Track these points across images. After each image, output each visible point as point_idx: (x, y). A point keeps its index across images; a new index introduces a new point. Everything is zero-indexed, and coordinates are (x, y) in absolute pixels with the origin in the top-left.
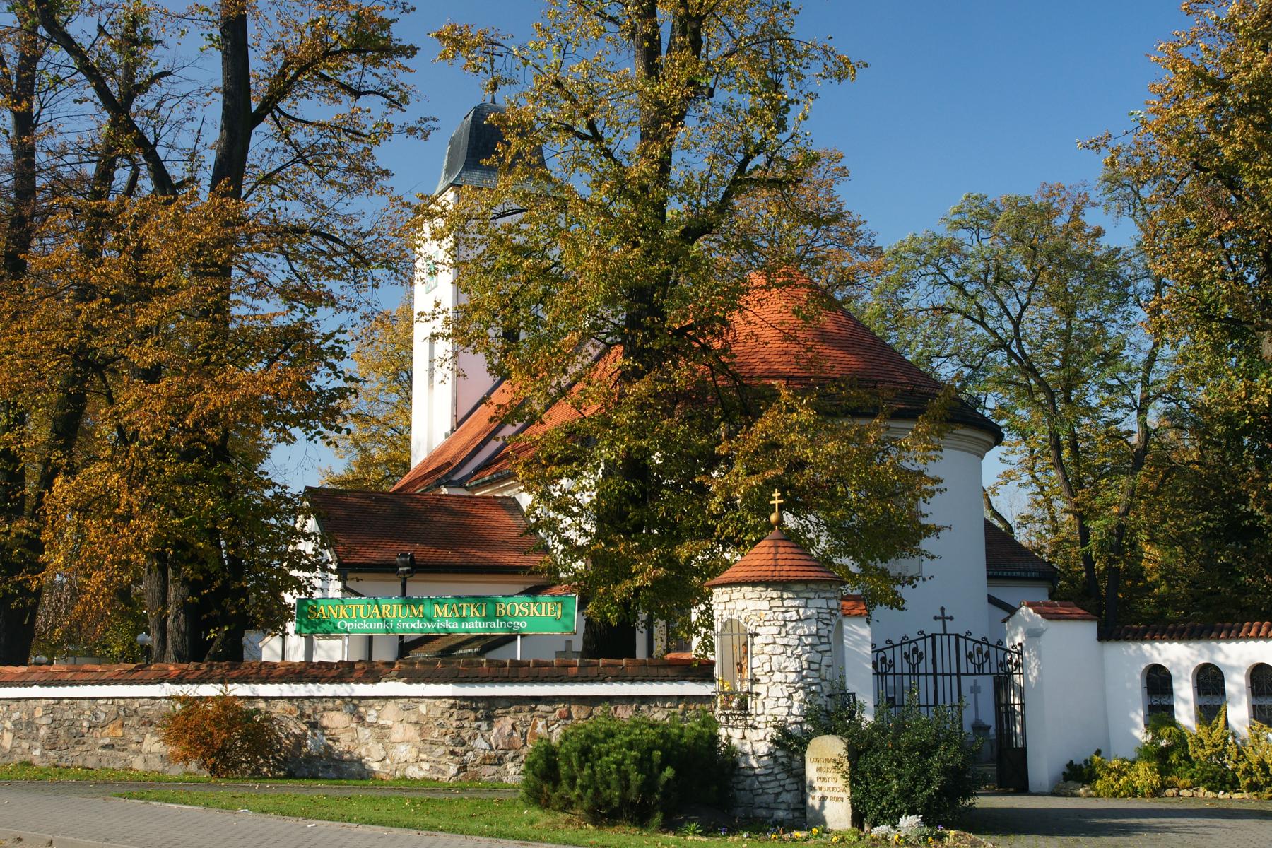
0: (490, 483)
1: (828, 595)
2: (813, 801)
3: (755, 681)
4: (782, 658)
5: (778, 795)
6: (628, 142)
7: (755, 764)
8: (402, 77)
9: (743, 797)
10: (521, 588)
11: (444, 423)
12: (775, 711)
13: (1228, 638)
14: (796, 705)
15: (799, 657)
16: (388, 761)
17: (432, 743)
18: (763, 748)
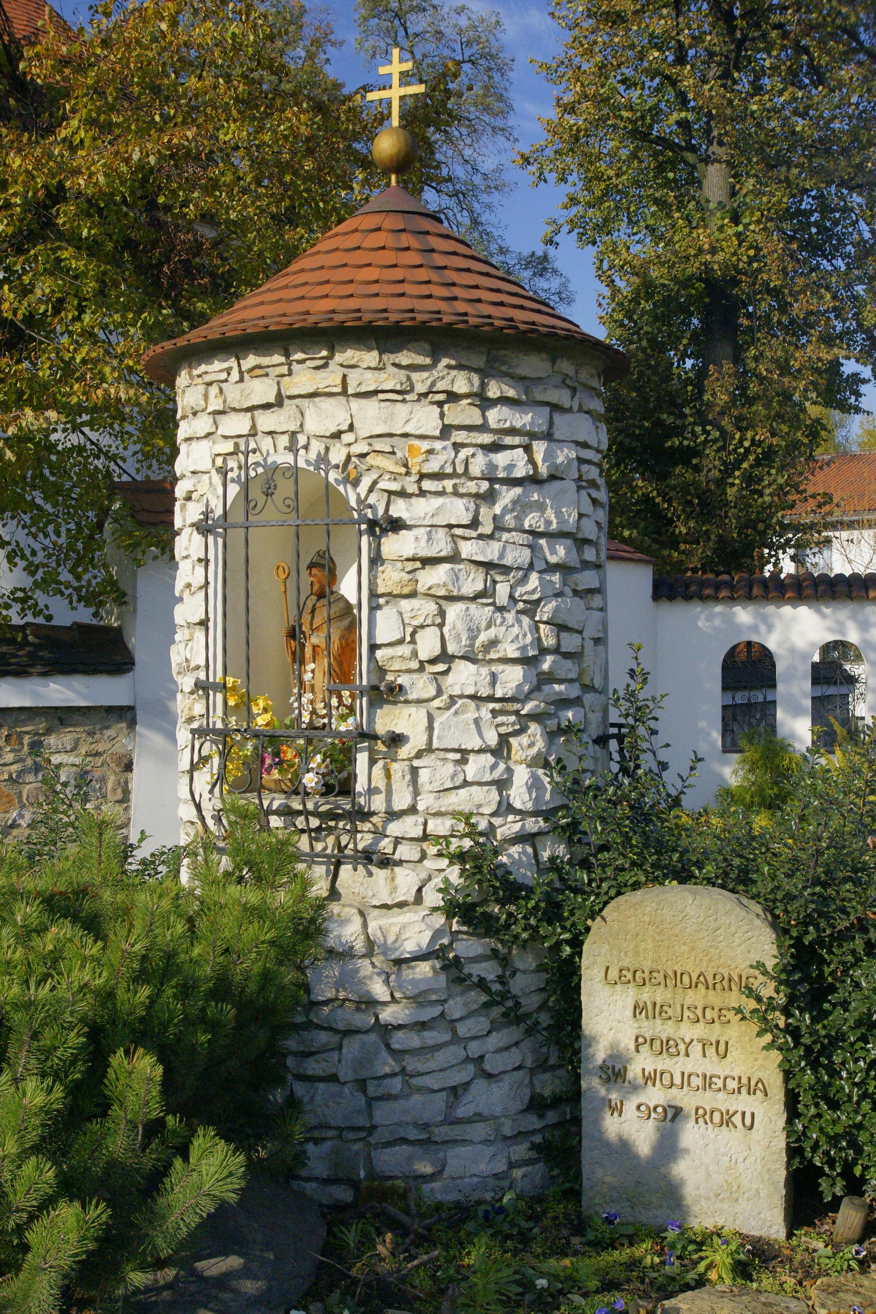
2: (629, 1125)
3: (385, 693)
4: (482, 613)
5: (456, 1092)
7: (379, 990)
9: (329, 1105)
12: (460, 800)
14: (521, 775)
15: (531, 608)
18: (415, 931)
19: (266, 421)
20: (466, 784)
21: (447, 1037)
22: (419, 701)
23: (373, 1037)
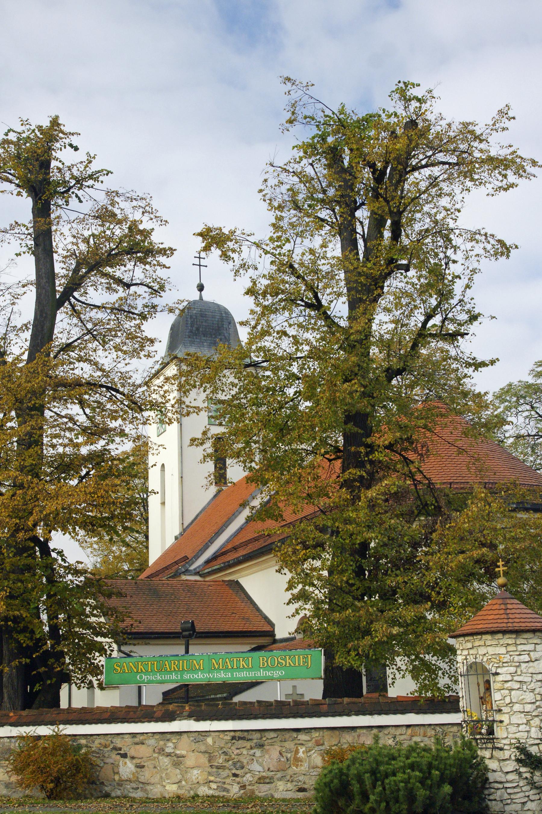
0: (220, 570)
1: (535, 642)
5: (524, 803)
6: (340, 309)
8: (161, 273)
10: (248, 648)
11: (174, 529)
12: (518, 735)
13: (116, 707)
16: (183, 783)
17: (218, 768)
19: (471, 652)
20: (519, 731)
21: (520, 790)
22: (507, 713)
23: (503, 790)
